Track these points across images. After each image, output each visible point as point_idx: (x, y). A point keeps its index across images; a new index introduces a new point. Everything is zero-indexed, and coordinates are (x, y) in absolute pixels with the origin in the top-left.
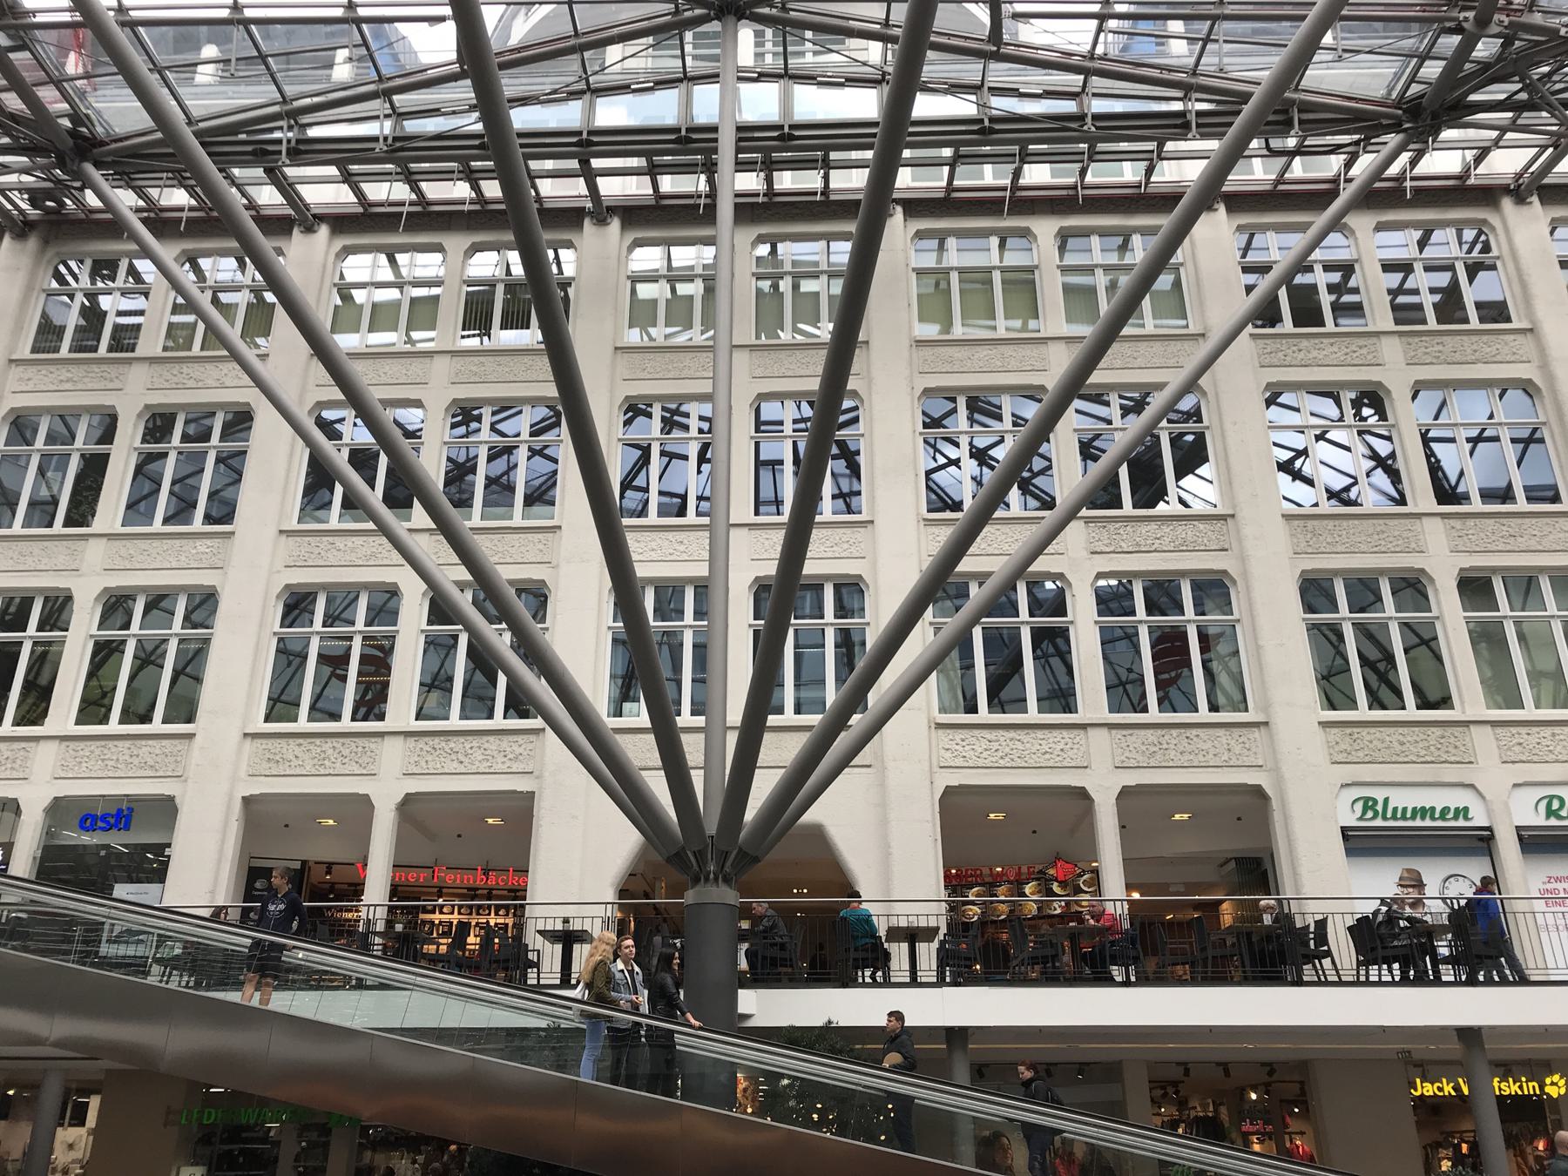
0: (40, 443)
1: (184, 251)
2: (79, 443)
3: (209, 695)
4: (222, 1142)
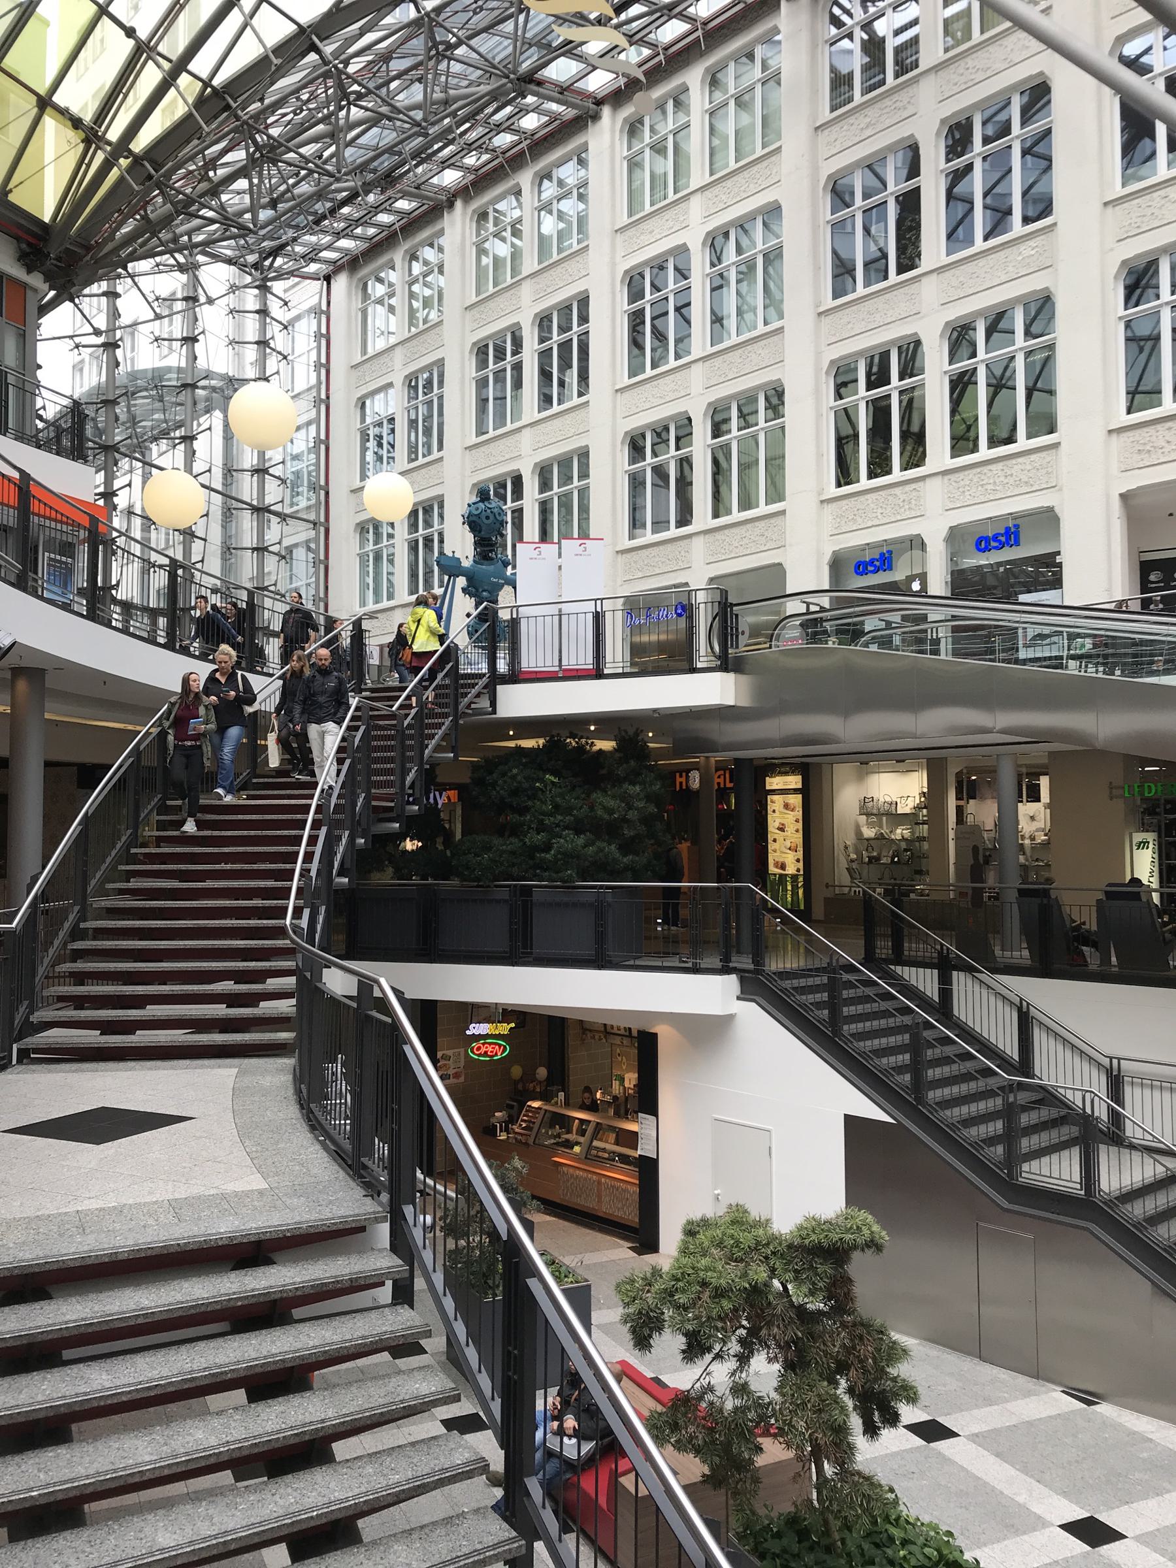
0: (859, 201)
1: (535, 173)
2: (891, 187)
3: (1065, 405)
4: (1167, 812)
